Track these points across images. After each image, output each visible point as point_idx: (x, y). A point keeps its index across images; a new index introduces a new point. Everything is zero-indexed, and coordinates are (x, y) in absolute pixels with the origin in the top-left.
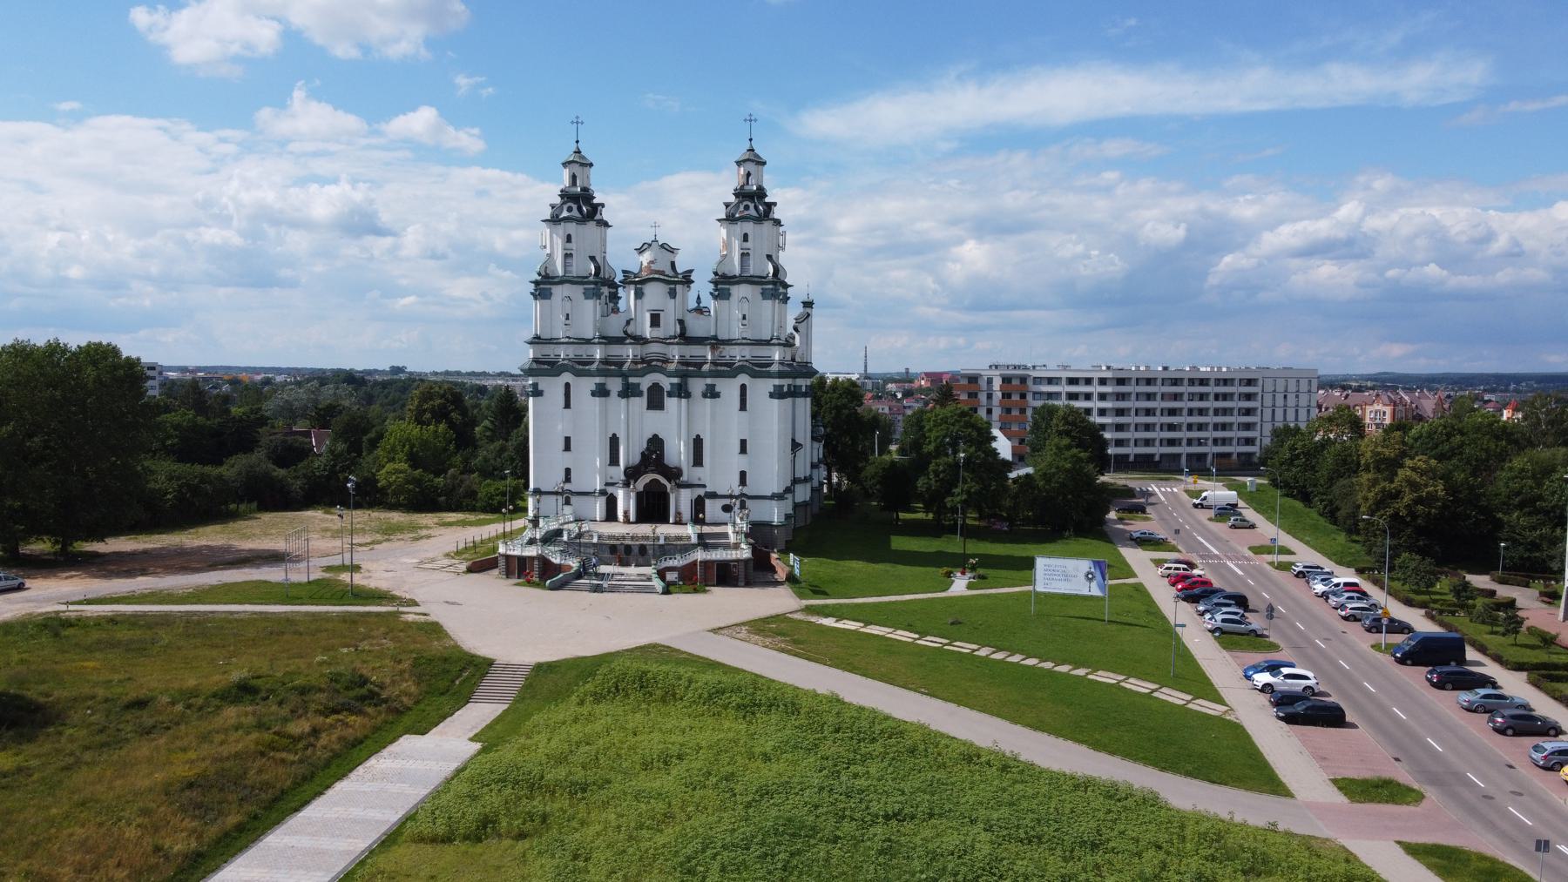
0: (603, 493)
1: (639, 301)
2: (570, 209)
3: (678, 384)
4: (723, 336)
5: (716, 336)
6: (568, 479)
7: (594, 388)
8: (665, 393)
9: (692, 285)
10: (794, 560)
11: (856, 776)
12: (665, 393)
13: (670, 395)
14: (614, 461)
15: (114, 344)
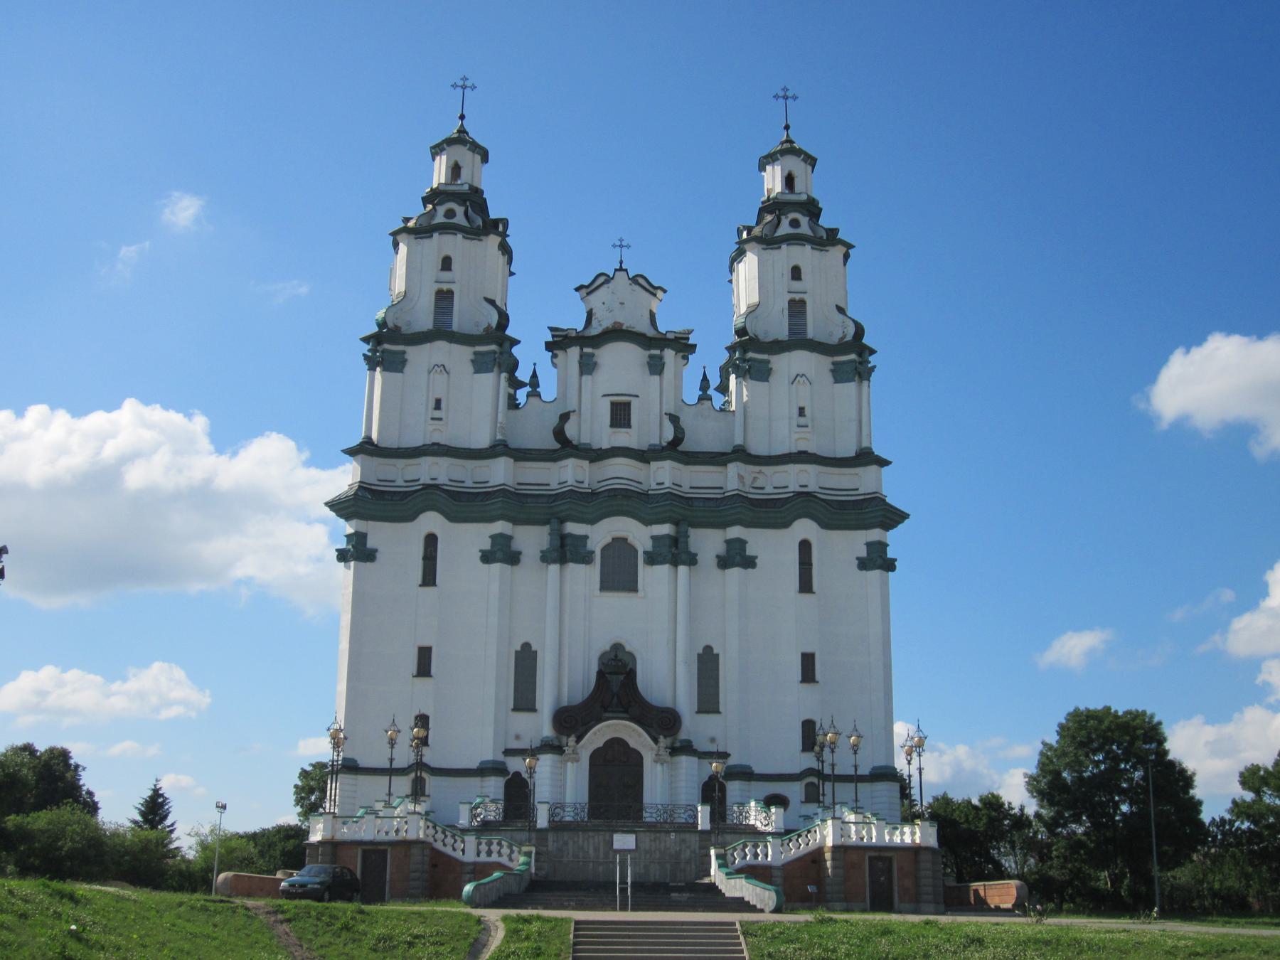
13: (652, 559)
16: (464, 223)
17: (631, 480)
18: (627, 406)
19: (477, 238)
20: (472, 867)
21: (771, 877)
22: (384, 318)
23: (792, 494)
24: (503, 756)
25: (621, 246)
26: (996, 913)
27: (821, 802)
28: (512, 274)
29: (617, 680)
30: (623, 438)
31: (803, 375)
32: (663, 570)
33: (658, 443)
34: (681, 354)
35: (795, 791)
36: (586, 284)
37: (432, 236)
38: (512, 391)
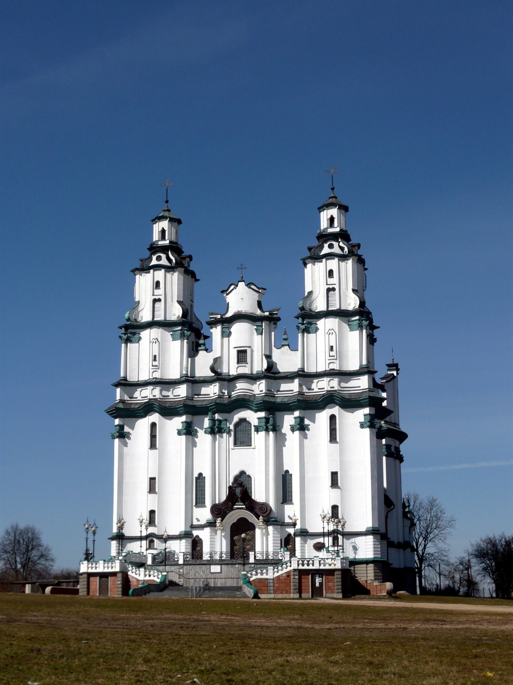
0: (186, 535)
1: (226, 339)
2: (159, 258)
3: (265, 418)
4: (311, 369)
5: (302, 370)
6: (152, 522)
7: (180, 427)
8: (253, 428)
9: (279, 323)
10: (465, 573)
11: (300, 632)
12: (253, 428)
13: (257, 429)
14: (200, 502)
15: (22, 526)
16: (166, 263)
17: (243, 389)
18: (245, 352)
19: (172, 270)
20: (142, 582)
21: (268, 587)
22: (129, 316)
23: (326, 392)
24: (190, 528)
25: (242, 268)
26: (445, 598)
27: (341, 546)
28: (366, 269)
29: (238, 491)
30: (245, 370)
31: (332, 329)
32: (262, 434)
33: (261, 370)
34: (272, 322)
35: (328, 541)
36: (226, 290)
37: (150, 272)
38: (371, 332)
